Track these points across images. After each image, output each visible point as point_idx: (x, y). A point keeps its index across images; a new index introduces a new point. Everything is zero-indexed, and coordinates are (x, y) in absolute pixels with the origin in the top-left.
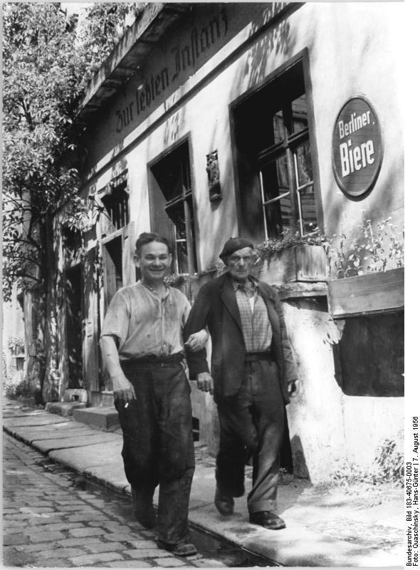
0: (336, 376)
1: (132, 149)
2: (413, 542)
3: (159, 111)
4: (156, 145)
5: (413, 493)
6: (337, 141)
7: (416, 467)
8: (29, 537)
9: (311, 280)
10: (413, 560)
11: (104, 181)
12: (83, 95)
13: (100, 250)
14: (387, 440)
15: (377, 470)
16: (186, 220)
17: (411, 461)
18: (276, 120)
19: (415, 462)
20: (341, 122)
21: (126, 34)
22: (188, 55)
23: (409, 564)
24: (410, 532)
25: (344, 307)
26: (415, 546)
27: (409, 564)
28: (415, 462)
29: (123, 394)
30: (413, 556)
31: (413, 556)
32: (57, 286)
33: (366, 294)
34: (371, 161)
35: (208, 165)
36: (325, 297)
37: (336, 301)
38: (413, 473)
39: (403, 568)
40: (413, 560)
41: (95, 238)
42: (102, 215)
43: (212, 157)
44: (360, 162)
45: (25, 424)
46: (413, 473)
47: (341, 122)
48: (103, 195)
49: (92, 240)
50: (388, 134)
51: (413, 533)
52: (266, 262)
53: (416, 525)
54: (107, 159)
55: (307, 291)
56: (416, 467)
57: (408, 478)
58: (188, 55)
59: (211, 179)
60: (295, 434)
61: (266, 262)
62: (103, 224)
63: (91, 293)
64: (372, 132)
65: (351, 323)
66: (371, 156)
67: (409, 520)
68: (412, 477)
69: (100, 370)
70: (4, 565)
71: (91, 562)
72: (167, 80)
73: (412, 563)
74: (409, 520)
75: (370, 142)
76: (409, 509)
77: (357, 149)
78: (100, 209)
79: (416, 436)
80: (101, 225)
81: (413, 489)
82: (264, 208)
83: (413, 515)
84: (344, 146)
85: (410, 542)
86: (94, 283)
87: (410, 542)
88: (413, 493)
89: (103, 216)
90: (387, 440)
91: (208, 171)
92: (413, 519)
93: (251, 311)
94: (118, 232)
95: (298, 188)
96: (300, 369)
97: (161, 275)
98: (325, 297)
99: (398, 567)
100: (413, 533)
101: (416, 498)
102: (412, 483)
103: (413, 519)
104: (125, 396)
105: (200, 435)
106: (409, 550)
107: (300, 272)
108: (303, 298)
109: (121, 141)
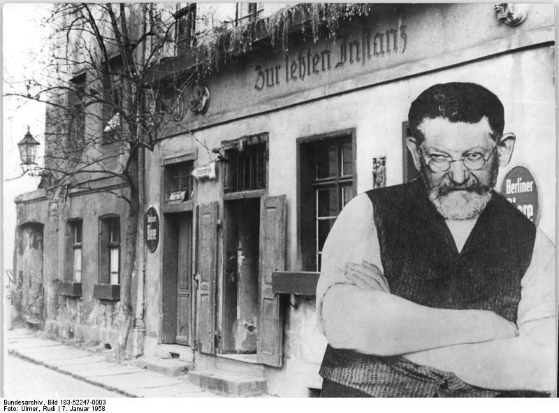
1: (470, 65)
2: (28, 406)
7: (91, 409)
10: (10, 406)
14: (44, 18)
18: (110, 56)
22: (272, 76)
23: (5, 402)
26: (23, 409)
30: (13, 406)
31: (13, 406)
35: (374, 168)
39: (3, 396)
40: (10, 406)
58: (272, 76)
67: (49, 402)
69: (216, 333)
70: (297, 139)
71: (404, 43)
73: (7, 405)
74: (49, 402)
76: (59, 402)
82: (317, 222)
85: (27, 403)
87: (27, 403)
90: (44, 18)
91: (375, 176)
94: (249, 193)
96: (213, 394)
99: (3, 335)
106: (19, 403)
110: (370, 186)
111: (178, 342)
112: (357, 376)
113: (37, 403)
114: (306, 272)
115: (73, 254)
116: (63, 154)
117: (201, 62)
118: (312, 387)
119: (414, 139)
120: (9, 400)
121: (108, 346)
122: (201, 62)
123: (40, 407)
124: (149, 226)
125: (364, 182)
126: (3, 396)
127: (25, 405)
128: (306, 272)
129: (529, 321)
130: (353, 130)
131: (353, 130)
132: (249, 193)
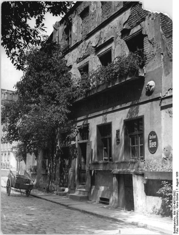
0: (145, 191)
2: (176, 224)
3: (101, 112)
4: (100, 121)
5: (176, 203)
6: (149, 139)
7: (177, 192)
10: (176, 231)
11: (80, 124)
12: (76, 98)
13: (77, 145)
15: (152, 211)
17: (175, 190)
19: (177, 190)
20: (150, 135)
21: (93, 89)
23: (174, 233)
24: (175, 219)
25: (147, 177)
26: (177, 225)
27: (174, 233)
28: (177, 190)
30: (176, 229)
31: (176, 229)
32: (57, 152)
33: (152, 175)
34: (155, 146)
36: (144, 174)
37: (146, 176)
38: (176, 195)
40: (176, 231)
41: (75, 141)
42: (78, 134)
43: (118, 131)
44: (153, 146)
46: (176, 195)
47: (150, 135)
48: (79, 128)
49: (74, 141)
50: (159, 142)
51: (176, 220)
52: (131, 164)
53: (177, 216)
54: (82, 118)
55: (140, 172)
56: (177, 192)
57: (174, 197)
59: (117, 135)
60: (136, 211)
61: (131, 164)
62: (78, 136)
64: (155, 140)
65: (148, 181)
66: (156, 145)
68: (176, 197)
72: (71, 41)
74: (175, 214)
75: (156, 142)
76: (174, 210)
77: (153, 143)
78: (78, 132)
79: (177, 180)
80: (78, 137)
81: (176, 202)
83: (176, 212)
84: (150, 141)
85: (175, 224)
87: (175, 224)
88: (176, 203)
89: (78, 134)
91: (116, 134)
92: (176, 214)
94: (85, 141)
95: (140, 145)
98: (144, 174)
100: (176, 220)
101: (178, 205)
102: (176, 199)
103: (176, 214)
105: (109, 204)
106: (175, 227)
107: (139, 168)
108: (139, 174)
109: (88, 115)
110: (100, 196)
116: (42, 41)
117: (21, 132)
118: (113, 123)
119: (55, 98)
121: (44, 188)
122: (21, 132)
124: (150, 141)
127: (176, 225)
132: (85, 141)
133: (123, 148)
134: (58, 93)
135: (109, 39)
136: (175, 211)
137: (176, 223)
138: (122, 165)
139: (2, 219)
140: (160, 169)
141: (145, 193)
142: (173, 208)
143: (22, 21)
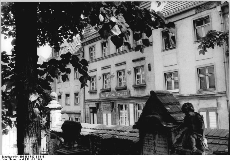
2: (11, 158)
8: (213, 48)
9: (169, 15)
10: (4, 158)
16: (41, 69)
23: (2, 156)
27: (2, 156)
29: (170, 85)
30: (5, 158)
31: (5, 158)
39: (1, 154)
40: (4, 158)
45: (202, 61)
63: (25, 140)
74: (20, 157)
76: (24, 156)
85: (11, 157)
86: (38, 136)
87: (11, 157)
93: (167, 107)
97: (194, 139)
101: (12, 160)
104: (170, 85)
106: (8, 157)
111: (217, 3)
112: (75, 50)
113: (15, 157)
114: (140, 17)
115: (207, 127)
120: (4, 156)
123: (16, 159)
125: (186, 150)
126: (1, 154)
127: (10, 158)
128: (140, 17)
129: (92, 129)
130: (69, 94)
131: (69, 94)
133: (133, 73)
134: (7, 30)
135: (206, 15)
136: (23, 157)
137: (12, 158)
138: (106, 82)
139: (228, 38)
140: (119, 88)
141: (17, 152)
142: (26, 155)
143: (136, 31)
